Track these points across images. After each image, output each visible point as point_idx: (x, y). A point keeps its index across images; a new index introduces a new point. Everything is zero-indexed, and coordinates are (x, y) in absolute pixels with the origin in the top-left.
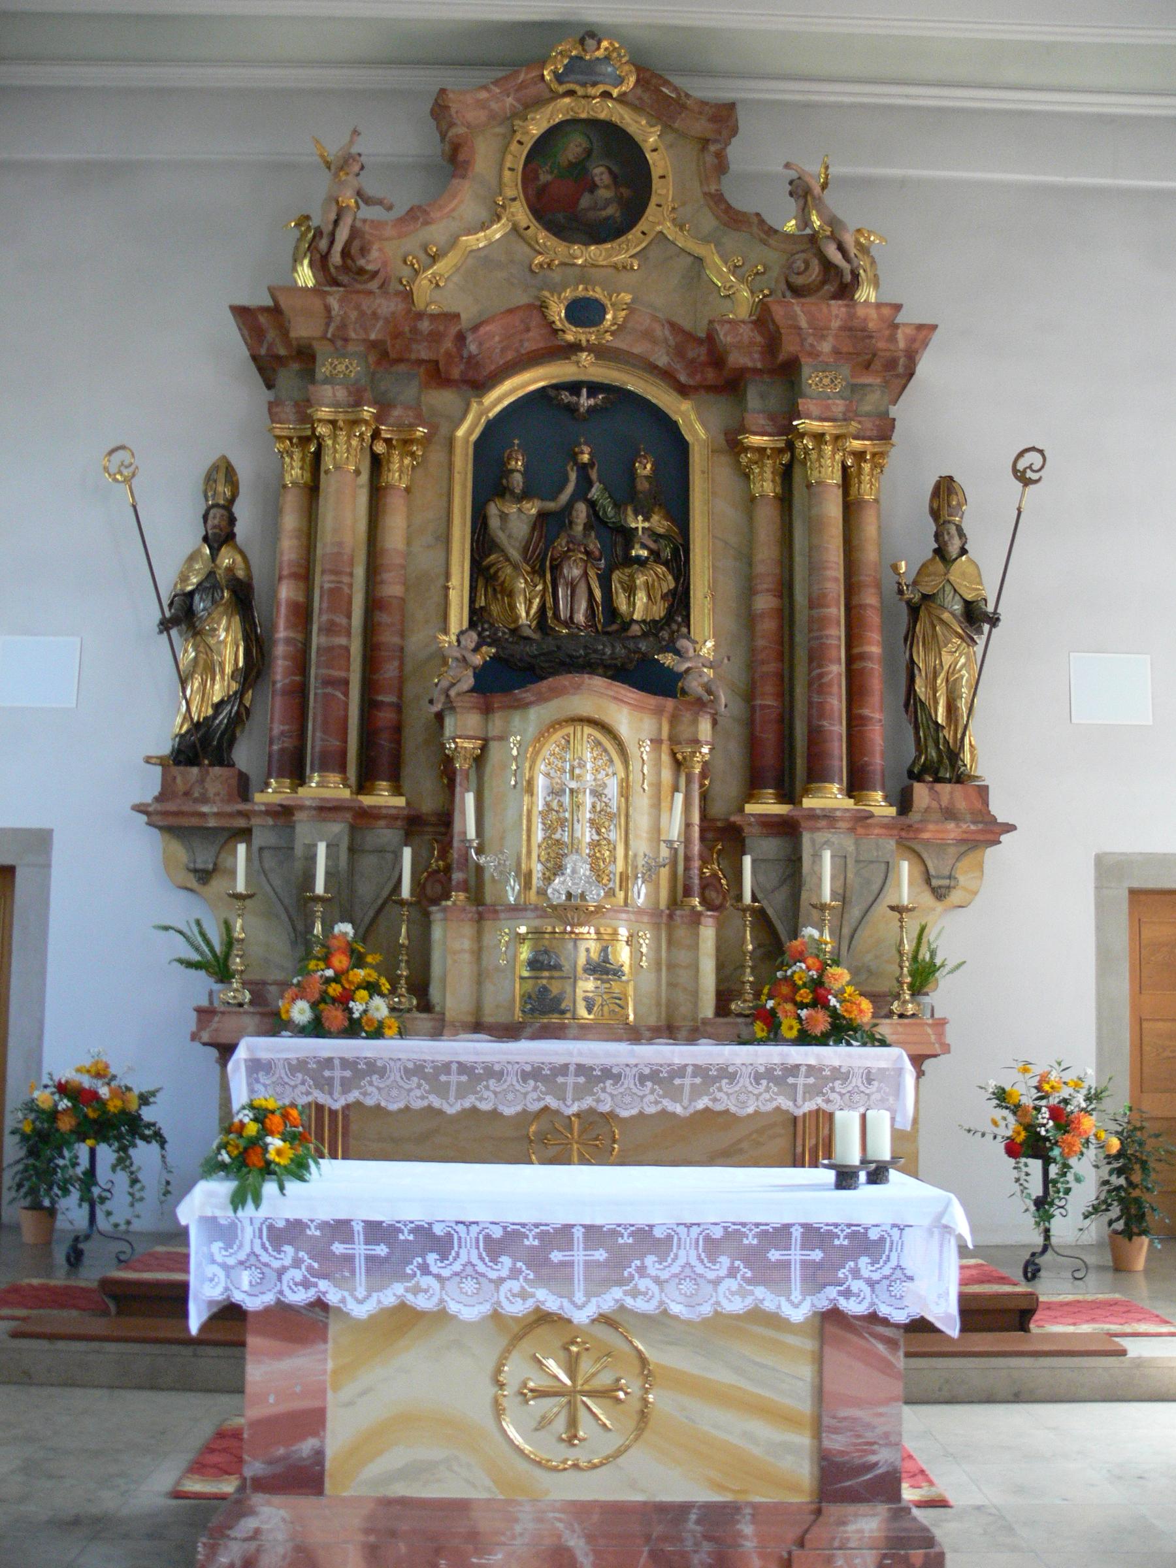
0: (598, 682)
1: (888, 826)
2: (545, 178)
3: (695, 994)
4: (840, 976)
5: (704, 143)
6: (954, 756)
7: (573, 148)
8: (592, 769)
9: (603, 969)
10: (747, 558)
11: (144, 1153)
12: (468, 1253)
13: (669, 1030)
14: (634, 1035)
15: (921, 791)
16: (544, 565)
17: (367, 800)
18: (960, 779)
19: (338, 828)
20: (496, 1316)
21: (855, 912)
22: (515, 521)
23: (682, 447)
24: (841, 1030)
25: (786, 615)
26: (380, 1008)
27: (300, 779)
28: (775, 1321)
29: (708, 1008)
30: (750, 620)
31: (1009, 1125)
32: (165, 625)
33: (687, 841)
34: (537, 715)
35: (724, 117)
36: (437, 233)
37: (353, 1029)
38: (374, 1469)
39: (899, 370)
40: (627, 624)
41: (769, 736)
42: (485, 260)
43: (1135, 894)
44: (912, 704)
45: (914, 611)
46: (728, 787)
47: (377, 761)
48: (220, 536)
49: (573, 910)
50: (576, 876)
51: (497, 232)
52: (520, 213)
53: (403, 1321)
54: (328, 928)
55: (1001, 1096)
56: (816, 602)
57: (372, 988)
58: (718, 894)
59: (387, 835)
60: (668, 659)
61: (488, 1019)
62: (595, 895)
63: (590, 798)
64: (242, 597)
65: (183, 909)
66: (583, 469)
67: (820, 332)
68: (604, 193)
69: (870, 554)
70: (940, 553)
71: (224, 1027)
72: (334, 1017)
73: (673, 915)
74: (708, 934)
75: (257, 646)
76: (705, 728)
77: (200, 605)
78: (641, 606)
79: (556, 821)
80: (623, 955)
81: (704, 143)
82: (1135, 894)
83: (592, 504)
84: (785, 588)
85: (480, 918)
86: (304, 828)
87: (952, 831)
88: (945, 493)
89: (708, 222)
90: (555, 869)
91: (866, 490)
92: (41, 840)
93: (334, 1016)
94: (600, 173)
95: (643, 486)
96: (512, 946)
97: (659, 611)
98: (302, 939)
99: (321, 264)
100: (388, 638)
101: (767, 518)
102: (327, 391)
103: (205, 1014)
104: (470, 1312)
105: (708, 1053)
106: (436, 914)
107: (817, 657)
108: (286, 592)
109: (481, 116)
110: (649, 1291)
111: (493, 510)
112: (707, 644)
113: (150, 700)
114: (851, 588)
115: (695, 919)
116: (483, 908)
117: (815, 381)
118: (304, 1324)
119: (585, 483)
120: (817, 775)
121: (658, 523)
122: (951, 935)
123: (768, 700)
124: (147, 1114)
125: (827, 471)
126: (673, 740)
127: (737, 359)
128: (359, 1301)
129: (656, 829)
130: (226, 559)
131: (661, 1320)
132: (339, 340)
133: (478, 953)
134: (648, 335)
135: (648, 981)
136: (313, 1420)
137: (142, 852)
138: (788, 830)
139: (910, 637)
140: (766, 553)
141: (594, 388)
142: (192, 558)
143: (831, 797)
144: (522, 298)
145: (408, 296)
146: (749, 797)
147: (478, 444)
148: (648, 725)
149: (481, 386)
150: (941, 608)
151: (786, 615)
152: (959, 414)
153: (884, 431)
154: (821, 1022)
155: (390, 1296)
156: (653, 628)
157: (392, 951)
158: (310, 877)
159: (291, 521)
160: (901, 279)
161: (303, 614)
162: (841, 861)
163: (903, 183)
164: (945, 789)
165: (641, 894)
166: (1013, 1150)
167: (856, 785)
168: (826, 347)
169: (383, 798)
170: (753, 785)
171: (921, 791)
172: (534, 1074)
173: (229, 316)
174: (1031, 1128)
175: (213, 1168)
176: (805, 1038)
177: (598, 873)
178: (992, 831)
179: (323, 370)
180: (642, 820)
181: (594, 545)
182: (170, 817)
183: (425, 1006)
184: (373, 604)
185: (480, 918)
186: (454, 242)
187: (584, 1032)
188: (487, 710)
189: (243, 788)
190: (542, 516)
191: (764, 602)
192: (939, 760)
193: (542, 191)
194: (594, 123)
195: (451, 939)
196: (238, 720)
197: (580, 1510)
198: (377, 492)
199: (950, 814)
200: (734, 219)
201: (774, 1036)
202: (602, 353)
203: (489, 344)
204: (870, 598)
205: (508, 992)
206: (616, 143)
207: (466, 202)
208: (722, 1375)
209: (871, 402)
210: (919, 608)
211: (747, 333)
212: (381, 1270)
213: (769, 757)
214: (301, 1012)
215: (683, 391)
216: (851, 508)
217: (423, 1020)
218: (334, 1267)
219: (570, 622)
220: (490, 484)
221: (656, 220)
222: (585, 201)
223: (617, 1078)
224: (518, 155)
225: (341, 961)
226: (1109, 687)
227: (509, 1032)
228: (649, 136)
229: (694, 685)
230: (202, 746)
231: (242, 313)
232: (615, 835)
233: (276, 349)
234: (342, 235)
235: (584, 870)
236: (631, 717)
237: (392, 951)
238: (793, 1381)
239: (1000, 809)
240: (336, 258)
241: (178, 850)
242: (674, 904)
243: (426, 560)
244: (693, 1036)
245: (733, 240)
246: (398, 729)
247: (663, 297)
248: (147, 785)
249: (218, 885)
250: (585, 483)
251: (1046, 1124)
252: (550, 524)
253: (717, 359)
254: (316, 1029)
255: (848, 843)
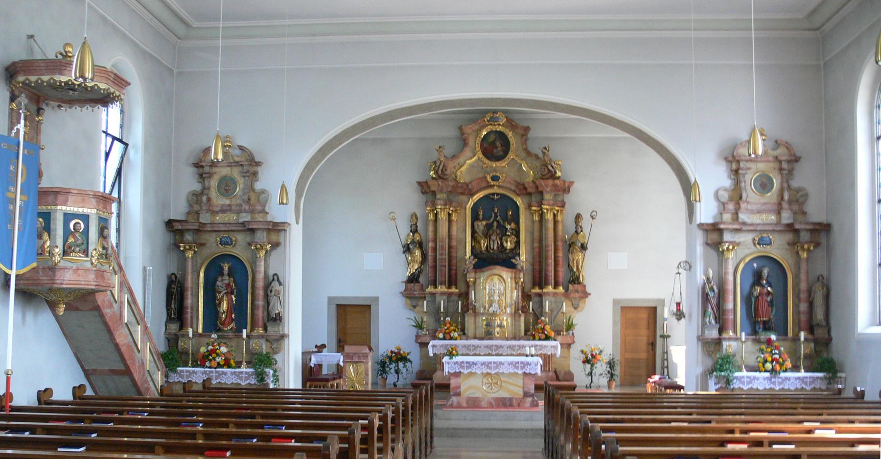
0: (499, 267)
1: (563, 295)
2: (485, 145)
3: (520, 331)
4: (548, 327)
5: (523, 135)
6: (578, 278)
7: (492, 138)
8: (498, 285)
9: (500, 326)
10: (532, 233)
11: (408, 364)
12: (479, 365)
13: (515, 338)
14: (507, 339)
15: (571, 286)
16: (487, 235)
17: (450, 290)
18: (579, 283)
19: (445, 297)
20: (482, 373)
21: (555, 313)
22: (481, 225)
23: (517, 208)
24: (547, 338)
25: (541, 248)
26: (456, 334)
27: (436, 288)
28: (517, 374)
29: (523, 333)
30: (533, 248)
31: (583, 357)
32: (404, 252)
33: (420, 415)
34: (486, 274)
35: (527, 129)
36: (461, 160)
37: (451, 339)
38: (469, 392)
39: (566, 190)
40: (506, 249)
41: (537, 275)
42: (472, 166)
43: (622, 308)
44: (570, 268)
45: (570, 245)
46: (528, 285)
47: (451, 282)
48: (414, 231)
49: (494, 314)
50: (495, 307)
51: (476, 158)
52: (481, 156)
53: (471, 374)
54: (444, 319)
55: (582, 352)
56: (547, 246)
57: (455, 331)
58: (525, 310)
59: (455, 298)
60: (514, 261)
61: (477, 336)
62: (499, 311)
63: (498, 290)
64: (420, 245)
65: (412, 315)
66: (496, 214)
67: (547, 186)
68: (499, 149)
69: (560, 233)
70: (576, 232)
71: (424, 340)
72: (447, 336)
73: (515, 315)
74: (522, 318)
75: (424, 256)
76: (522, 275)
77: (411, 247)
78: (509, 245)
79: (491, 295)
80: (505, 323)
81: (523, 135)
82: (622, 308)
83: (498, 222)
84: (541, 241)
85: (475, 316)
86: (438, 298)
87: (577, 295)
88: (578, 217)
89: (523, 155)
90: (491, 306)
91: (559, 218)
92: (376, 299)
93: (447, 336)
94: (498, 144)
95: (509, 217)
96: (482, 321)
97: (513, 246)
98: (438, 320)
99: (436, 172)
100: (454, 255)
101: (537, 225)
102: (439, 202)
103: (417, 337)
104: (479, 372)
105: (522, 342)
106: (466, 315)
107: (547, 258)
108: (431, 245)
109: (470, 131)
110: (501, 370)
111: (475, 224)
112: (523, 257)
113: (400, 269)
114: (555, 241)
115: (520, 315)
116: (476, 313)
117: (547, 197)
118: (457, 375)
119: (496, 216)
120: (547, 284)
121: (513, 225)
122: (578, 318)
123: (537, 267)
124: (408, 357)
125: (549, 217)
126: (515, 278)
127: (529, 190)
128: (465, 371)
129: (512, 297)
130: (416, 235)
131: (503, 373)
132: (441, 191)
133: (475, 322)
134: (510, 183)
135: (510, 329)
136: (459, 387)
137: (399, 302)
138: (540, 295)
139: (569, 251)
140: (536, 234)
141: (498, 194)
142: (408, 235)
143: (550, 289)
144: (481, 175)
145: (455, 180)
146: (533, 288)
147: (472, 209)
148: (509, 275)
149: (472, 195)
150: (575, 245)
151: (541, 248)
152: (584, 196)
153: (563, 205)
154: (543, 336)
155: (469, 370)
156: (512, 250)
157: (457, 323)
158: (439, 308)
159: (431, 228)
160: (569, 166)
161: (435, 249)
162: (551, 302)
163: (571, 138)
164: (576, 286)
165: (508, 310)
166: (584, 362)
167: (556, 286)
168: (548, 189)
169: (454, 290)
170: (534, 285)
171: (571, 286)
172: (487, 347)
173: (416, 185)
174: (587, 358)
175: (446, 355)
176: (540, 339)
177: (499, 307)
178: (586, 295)
179: (438, 196)
180: (508, 295)
181: (498, 231)
182: (408, 295)
183: (464, 334)
184: (450, 247)
185: (475, 316)
186: (465, 162)
187: (497, 339)
188: (476, 272)
189: (422, 289)
190: (487, 224)
191: (536, 245)
192: (575, 280)
193: (485, 149)
194: (496, 131)
195: (469, 321)
196: (420, 272)
197: (493, 398)
198: (450, 221)
199: (577, 291)
200: (529, 153)
201: (534, 339)
202: (499, 186)
203: (474, 186)
204: (560, 243)
205: (481, 331)
206: (502, 136)
207: (468, 152)
208: (511, 381)
209: (560, 199)
210: (571, 245)
211: (531, 184)
212: (468, 368)
213: (537, 279)
214: (441, 336)
215: (518, 195)
216: (555, 222)
217: (463, 337)
218: (463, 367)
219: (493, 249)
220: (475, 218)
221: (511, 155)
222: (495, 151)
223: (530, 364)
224: (479, 140)
225: (448, 325)
226: (617, 260)
227: (482, 339)
228: (510, 134)
229: (519, 267)
230: (413, 279)
231: (419, 183)
232: (503, 298)
233: (424, 187)
234: (441, 167)
235: (497, 306)
236: (506, 274)
237: (457, 323)
238: (520, 382)
239: (588, 290)
240: (440, 172)
241: (409, 301)
242: (516, 312)
243: (461, 235)
244: (520, 339)
245: (529, 159)
246: (456, 274)
247: (513, 174)
248: (403, 287)
249: (418, 309)
250: (496, 216)
251: (590, 357)
252: (489, 226)
253: (525, 188)
254: (444, 338)
255: (553, 299)
